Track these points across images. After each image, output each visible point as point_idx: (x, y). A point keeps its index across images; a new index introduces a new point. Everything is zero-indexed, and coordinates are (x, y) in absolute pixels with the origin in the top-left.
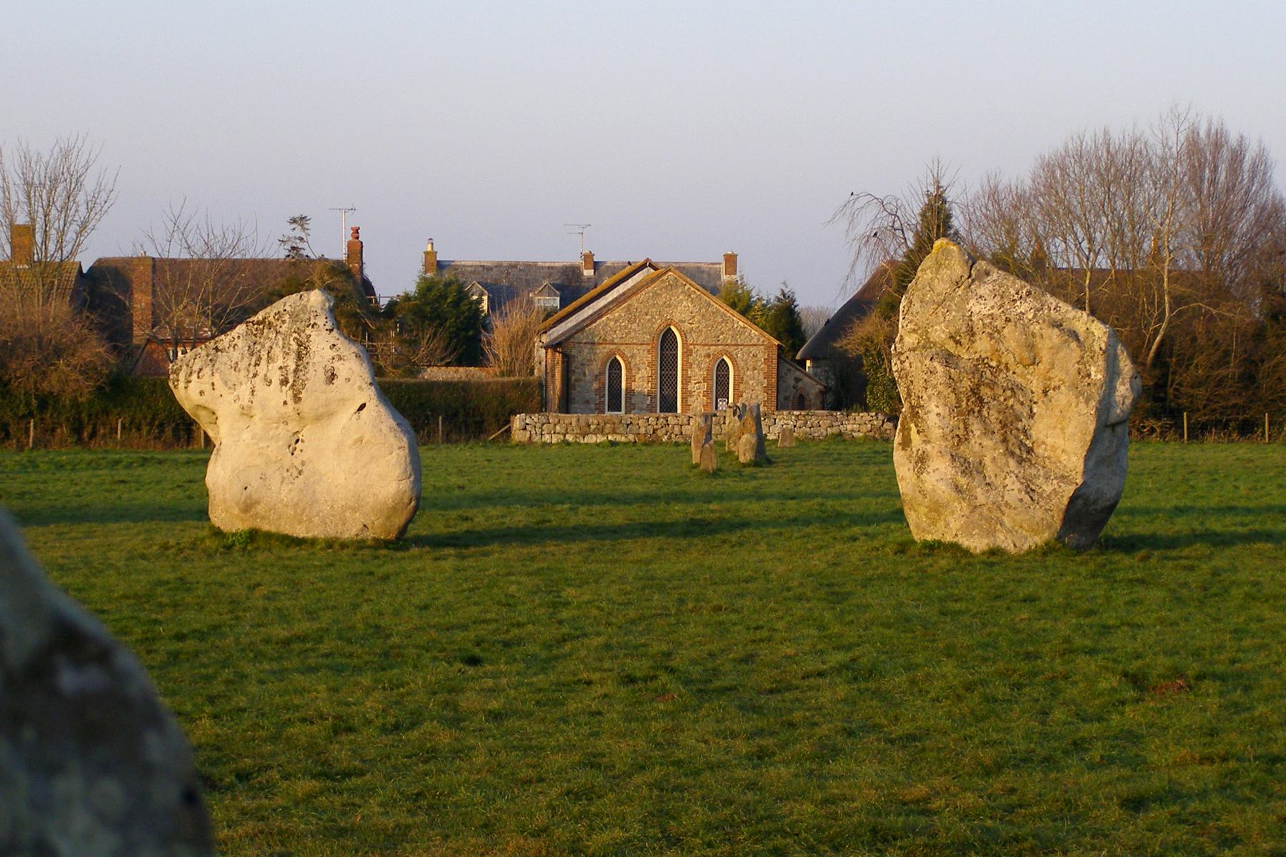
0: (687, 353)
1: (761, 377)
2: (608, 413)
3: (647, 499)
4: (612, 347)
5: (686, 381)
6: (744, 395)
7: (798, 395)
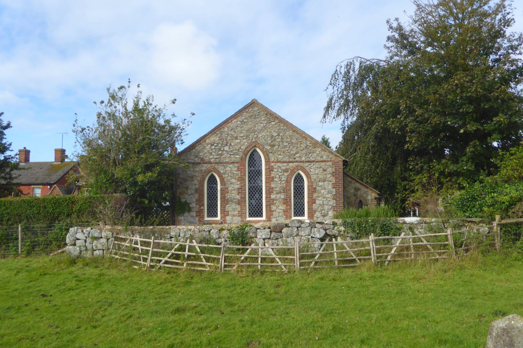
0: (270, 170)
1: (330, 187)
2: (294, 218)
3: (348, 267)
4: (209, 165)
5: (269, 191)
6: (317, 202)
7: (358, 201)
